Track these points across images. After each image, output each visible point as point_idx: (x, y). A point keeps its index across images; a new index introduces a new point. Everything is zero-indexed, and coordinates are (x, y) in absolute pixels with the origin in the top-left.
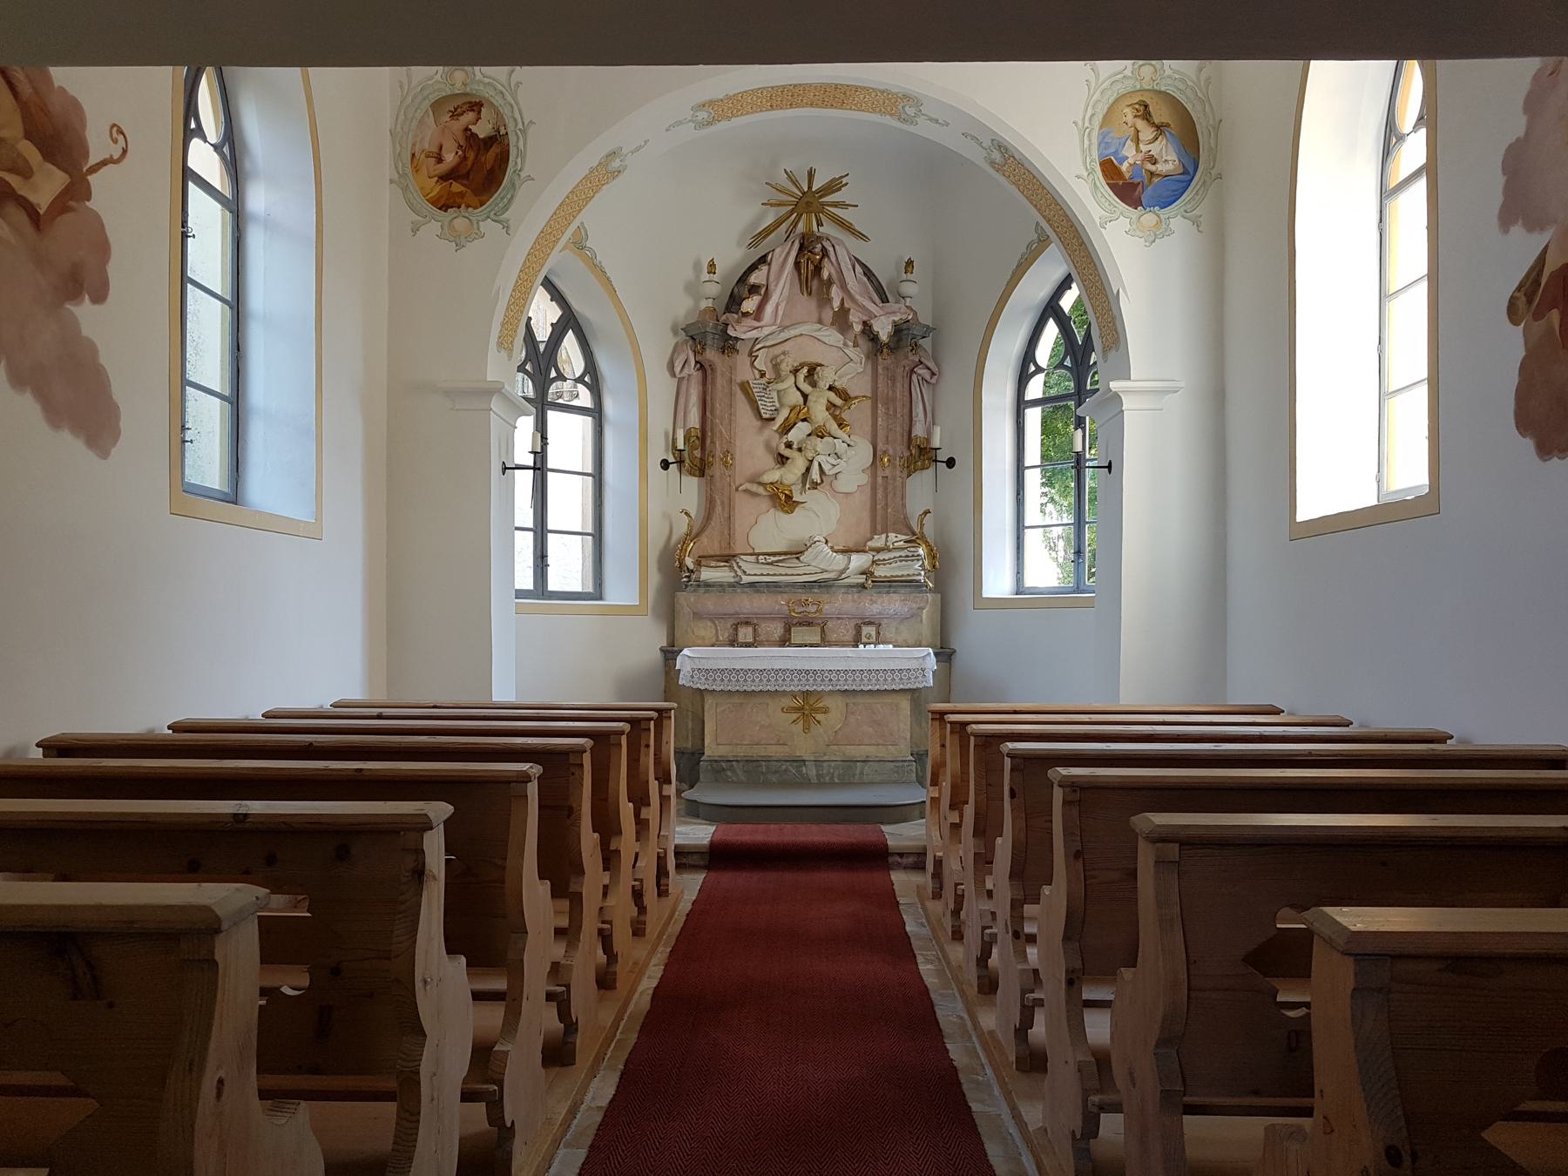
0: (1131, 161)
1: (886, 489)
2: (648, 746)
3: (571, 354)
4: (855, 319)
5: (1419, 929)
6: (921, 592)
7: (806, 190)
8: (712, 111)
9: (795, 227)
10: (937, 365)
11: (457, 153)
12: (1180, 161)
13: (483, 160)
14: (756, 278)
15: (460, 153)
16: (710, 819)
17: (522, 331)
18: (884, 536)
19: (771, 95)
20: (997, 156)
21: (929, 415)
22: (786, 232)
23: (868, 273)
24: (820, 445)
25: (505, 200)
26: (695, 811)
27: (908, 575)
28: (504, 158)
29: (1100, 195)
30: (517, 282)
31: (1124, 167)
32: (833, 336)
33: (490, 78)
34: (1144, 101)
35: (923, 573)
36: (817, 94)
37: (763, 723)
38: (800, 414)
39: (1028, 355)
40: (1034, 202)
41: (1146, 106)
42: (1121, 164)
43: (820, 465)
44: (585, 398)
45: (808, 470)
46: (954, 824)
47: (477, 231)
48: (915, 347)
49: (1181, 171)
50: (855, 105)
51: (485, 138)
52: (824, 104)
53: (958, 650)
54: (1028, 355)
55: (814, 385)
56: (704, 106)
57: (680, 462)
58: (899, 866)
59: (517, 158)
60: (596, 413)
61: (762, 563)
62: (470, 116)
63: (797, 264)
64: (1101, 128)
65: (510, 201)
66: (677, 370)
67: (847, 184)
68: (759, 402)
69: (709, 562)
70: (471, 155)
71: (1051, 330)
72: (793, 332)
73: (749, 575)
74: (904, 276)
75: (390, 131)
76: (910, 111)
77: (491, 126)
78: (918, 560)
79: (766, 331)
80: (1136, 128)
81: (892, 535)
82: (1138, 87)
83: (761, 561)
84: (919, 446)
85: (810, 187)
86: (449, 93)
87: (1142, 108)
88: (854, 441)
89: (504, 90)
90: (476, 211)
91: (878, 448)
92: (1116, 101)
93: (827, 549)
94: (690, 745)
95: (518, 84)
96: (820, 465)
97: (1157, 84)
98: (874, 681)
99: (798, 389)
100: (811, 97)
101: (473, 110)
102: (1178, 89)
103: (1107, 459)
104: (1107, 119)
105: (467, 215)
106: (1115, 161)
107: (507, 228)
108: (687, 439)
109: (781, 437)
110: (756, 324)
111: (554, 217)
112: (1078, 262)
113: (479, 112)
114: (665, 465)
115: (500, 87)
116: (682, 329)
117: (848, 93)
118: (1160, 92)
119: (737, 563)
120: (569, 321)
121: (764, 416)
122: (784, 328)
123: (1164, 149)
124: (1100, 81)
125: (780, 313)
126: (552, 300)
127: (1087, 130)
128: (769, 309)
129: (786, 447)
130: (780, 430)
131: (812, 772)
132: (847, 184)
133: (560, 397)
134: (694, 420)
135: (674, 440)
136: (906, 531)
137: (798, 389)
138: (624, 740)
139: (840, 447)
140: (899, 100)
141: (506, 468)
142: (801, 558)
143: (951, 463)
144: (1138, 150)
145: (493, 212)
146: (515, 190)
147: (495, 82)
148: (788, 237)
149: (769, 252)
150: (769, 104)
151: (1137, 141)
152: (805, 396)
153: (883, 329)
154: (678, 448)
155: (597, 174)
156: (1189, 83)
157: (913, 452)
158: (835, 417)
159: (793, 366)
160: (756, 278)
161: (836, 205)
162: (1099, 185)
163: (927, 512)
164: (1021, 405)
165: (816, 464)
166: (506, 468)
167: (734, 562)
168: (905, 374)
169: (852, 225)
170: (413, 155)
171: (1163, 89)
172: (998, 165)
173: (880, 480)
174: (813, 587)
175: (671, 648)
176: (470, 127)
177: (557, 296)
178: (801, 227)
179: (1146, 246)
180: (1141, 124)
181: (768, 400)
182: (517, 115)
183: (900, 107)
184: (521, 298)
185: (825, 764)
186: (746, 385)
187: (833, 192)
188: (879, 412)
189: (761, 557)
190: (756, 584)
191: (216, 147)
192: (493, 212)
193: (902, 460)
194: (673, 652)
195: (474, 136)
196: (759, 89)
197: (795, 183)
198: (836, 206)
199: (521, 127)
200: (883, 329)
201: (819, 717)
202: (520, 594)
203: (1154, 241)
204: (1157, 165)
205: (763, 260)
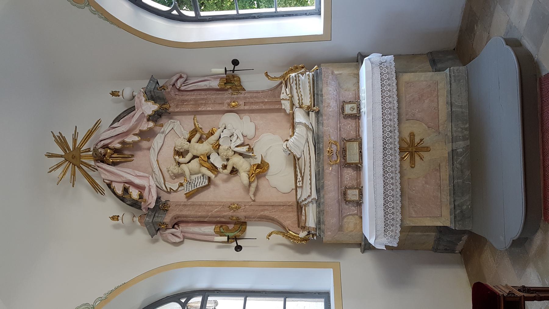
6: (321, 73)
7: (63, 159)
9: (90, 166)
14: (120, 192)
18: (283, 102)
23: (117, 120)
24: (224, 146)
37: (423, 182)
43: (237, 146)
45: (241, 154)
48: (163, 88)
53: (360, 51)
61: (302, 184)
63: (114, 164)
66: (178, 240)
68: (198, 187)
73: (311, 193)
74: (121, 96)
78: (299, 77)
81: (282, 96)
83: (301, 185)
85: (61, 156)
91: (226, 109)
93: (292, 140)
96: (237, 146)
108: (221, 234)
110: (147, 190)
121: (207, 183)
128: (137, 181)
136: (279, 88)
139: (226, 133)
143: (235, 62)
152: (194, 157)
153: (151, 108)
160: (120, 192)
161: (75, 140)
164: (198, 20)
174: (319, 148)
181: (197, 181)
188: (203, 109)
189: (298, 185)
194: (365, 245)
197: (58, 166)
200: (151, 108)
201: (417, 140)
205: (109, 185)
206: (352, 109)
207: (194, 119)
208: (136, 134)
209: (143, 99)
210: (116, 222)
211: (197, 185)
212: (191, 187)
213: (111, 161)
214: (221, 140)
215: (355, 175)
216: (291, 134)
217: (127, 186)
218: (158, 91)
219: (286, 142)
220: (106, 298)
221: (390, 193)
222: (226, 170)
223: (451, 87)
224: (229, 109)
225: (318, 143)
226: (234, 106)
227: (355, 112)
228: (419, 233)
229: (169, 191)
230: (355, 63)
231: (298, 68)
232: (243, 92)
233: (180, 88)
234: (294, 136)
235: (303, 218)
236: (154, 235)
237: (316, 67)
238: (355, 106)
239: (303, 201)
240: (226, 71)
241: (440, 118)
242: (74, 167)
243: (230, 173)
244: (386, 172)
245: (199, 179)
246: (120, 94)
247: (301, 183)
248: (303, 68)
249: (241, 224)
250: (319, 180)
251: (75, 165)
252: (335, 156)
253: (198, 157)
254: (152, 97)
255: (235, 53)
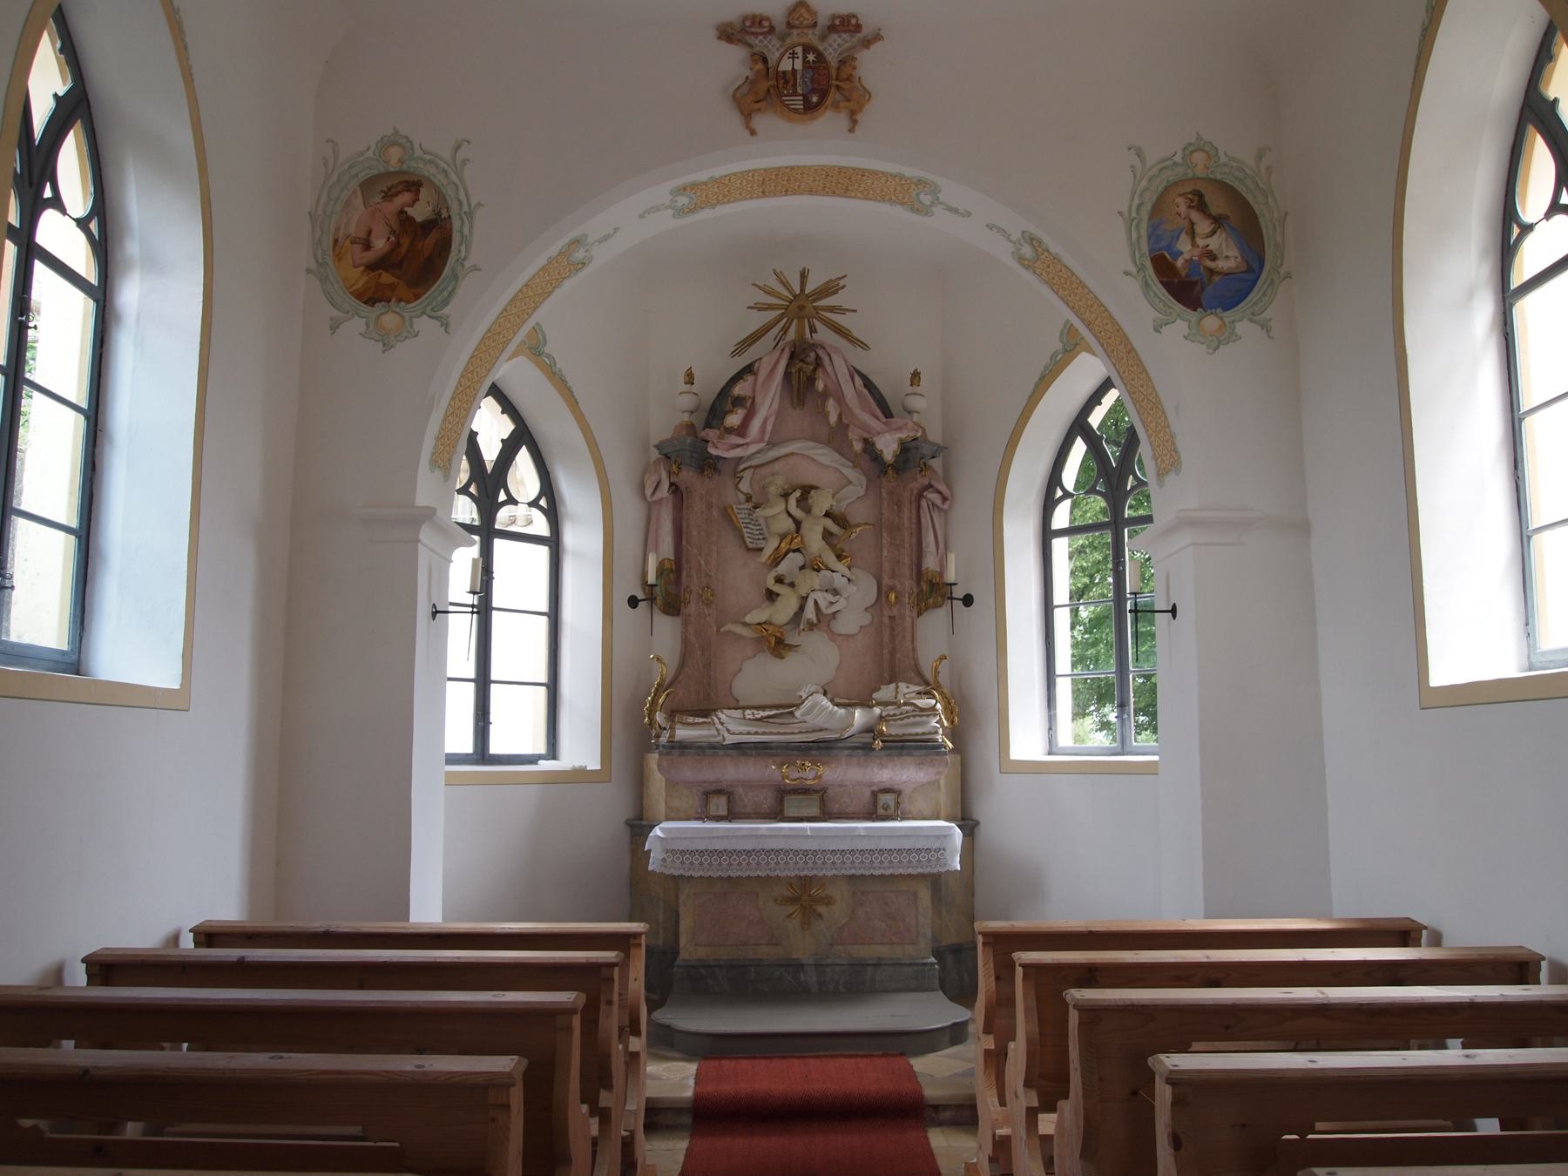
0: (1186, 256)
1: (893, 630)
2: (610, 1003)
3: (524, 477)
4: (854, 435)
5: (199, 192)
6: (939, 754)
7: (798, 292)
8: (693, 196)
9: (785, 333)
10: (950, 488)
11: (389, 238)
12: (1242, 257)
13: (420, 246)
14: (738, 390)
15: (393, 239)
16: (689, 1055)
17: (463, 445)
18: (892, 686)
19: (764, 180)
20: (1027, 250)
21: (942, 546)
22: (775, 339)
23: (868, 384)
24: (816, 580)
25: (445, 294)
26: (668, 1042)
27: (924, 734)
28: (444, 246)
29: (1152, 295)
30: (457, 388)
31: (1180, 263)
32: (825, 455)
33: (431, 154)
34: (1198, 191)
35: (941, 731)
36: (817, 178)
37: (751, 918)
38: (793, 541)
39: (1054, 479)
40: (1071, 304)
41: (1201, 196)
42: (1175, 259)
43: (816, 602)
44: (541, 526)
45: (802, 608)
46: (989, 1050)
47: (409, 329)
48: (925, 468)
49: (1245, 269)
50: (862, 192)
51: (422, 222)
52: (826, 191)
53: (982, 823)
54: (1054, 479)
55: (808, 510)
56: (685, 189)
57: (651, 599)
58: (940, 1124)
59: (461, 244)
60: (554, 543)
61: (749, 719)
62: (406, 197)
63: (787, 375)
64: (1150, 219)
65: (451, 294)
66: (649, 492)
67: (844, 286)
68: (745, 530)
69: (684, 717)
70: (406, 242)
71: (1079, 448)
72: (783, 451)
73: (733, 734)
74: (910, 389)
75: (310, 214)
76: (926, 199)
77: (430, 208)
78: (935, 715)
79: (753, 449)
80: (1190, 221)
82: (1191, 175)
83: (747, 717)
84: (931, 581)
85: (802, 290)
86: (382, 170)
87: (1196, 198)
88: (856, 576)
89: (447, 168)
90: (408, 306)
91: (884, 583)
92: (1167, 189)
93: (825, 702)
94: (660, 942)
95: (465, 161)
96: (816, 602)
97: (1212, 172)
98: (886, 864)
99: (790, 515)
100: (810, 182)
101: (411, 191)
102: (1236, 178)
103: (1168, 601)
104: (1157, 210)
105: (398, 310)
106: (1167, 255)
107: (446, 325)
108: (660, 572)
109: (770, 571)
110: (741, 441)
111: (505, 314)
112: (1124, 372)
113: (417, 192)
114: (633, 602)
115: (442, 164)
116: (655, 446)
117: (853, 179)
118: (1215, 181)
119: (719, 719)
120: (522, 437)
121: (751, 546)
122: (772, 444)
123: (1224, 245)
124: (1138, 178)
125: (769, 428)
126: (503, 413)
127: (1134, 223)
128: (756, 424)
129: (776, 582)
130: (769, 562)
131: (811, 978)
132: (844, 286)
133: (514, 522)
134: (667, 547)
135: (644, 574)
136: (917, 679)
137: (790, 515)
138: (576, 1021)
139: (839, 581)
140: (913, 186)
141: (437, 612)
142: (797, 714)
143: (968, 600)
144: (1194, 245)
145: (430, 307)
146: (457, 282)
147: (438, 160)
148: (777, 344)
149: (756, 361)
150: (761, 190)
151: (1192, 234)
152: (798, 523)
153: (888, 446)
154: (649, 583)
155: (556, 265)
156: (1248, 172)
157: (924, 587)
158: (833, 547)
159: (783, 489)
160: (738, 390)
161: (832, 309)
162: (1150, 282)
163: (943, 658)
164: (1047, 535)
165: (810, 604)
166: (437, 612)
167: (715, 718)
168: (913, 498)
169: (850, 331)
170: (336, 241)
171: (1219, 177)
172: (1027, 260)
173: (886, 620)
174: (810, 749)
175: (637, 822)
176: (406, 209)
177: (508, 407)
178: (792, 334)
179: (1209, 353)
180: (1195, 215)
181: (754, 527)
182: (462, 195)
183: (914, 195)
184: (464, 407)
185: (828, 969)
186: (730, 511)
187: (827, 296)
188: (884, 541)
189: (748, 712)
190: (743, 745)
191: (82, 223)
192: (430, 307)
193: (912, 597)
194: (642, 827)
195: (410, 219)
196: (750, 171)
197: (786, 285)
198: (832, 311)
199: (467, 210)
200: (888, 446)
201: (821, 909)
202: (453, 759)
203: (1217, 348)
204: (1217, 262)
205: (749, 369)
206: (885, 807)
207: (866, 524)
208: (841, 419)
209: (903, 435)
210: (681, 378)
211: (747, 528)
212: (743, 516)
213: (793, 371)
214: (828, 573)
215: (763, 811)
216: (837, 700)
217: (749, 405)
218: (918, 460)
219: (823, 692)
220: (554, 374)
221: (735, 860)
222: (773, 581)
223: (906, 964)
224: (884, 589)
225: (819, 748)
226: (888, 596)
227: (881, 811)
228: (661, 917)
229: (738, 475)
230: (960, 816)
231: (952, 713)
232: (915, 614)
233: (925, 497)
234: (831, 706)
235: (690, 719)
236: (658, 449)
237: (950, 745)
238: (891, 812)
239: (719, 719)
240: (952, 584)
241: (856, 947)
242: (782, 309)
243: (768, 589)
244: (768, 854)
245: (757, 532)
246: (916, 389)
247: (751, 717)
248: (952, 722)
249: (672, 607)
250: (756, 748)
251: (786, 309)
252: (796, 775)
253: (798, 531)
254: (906, 449)
255: (982, 598)
